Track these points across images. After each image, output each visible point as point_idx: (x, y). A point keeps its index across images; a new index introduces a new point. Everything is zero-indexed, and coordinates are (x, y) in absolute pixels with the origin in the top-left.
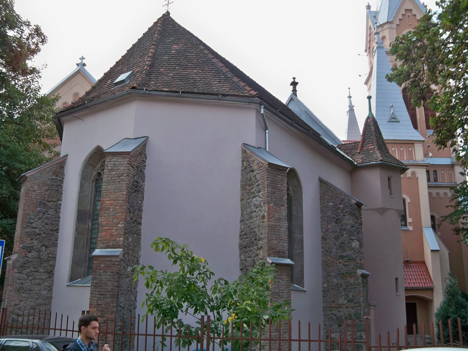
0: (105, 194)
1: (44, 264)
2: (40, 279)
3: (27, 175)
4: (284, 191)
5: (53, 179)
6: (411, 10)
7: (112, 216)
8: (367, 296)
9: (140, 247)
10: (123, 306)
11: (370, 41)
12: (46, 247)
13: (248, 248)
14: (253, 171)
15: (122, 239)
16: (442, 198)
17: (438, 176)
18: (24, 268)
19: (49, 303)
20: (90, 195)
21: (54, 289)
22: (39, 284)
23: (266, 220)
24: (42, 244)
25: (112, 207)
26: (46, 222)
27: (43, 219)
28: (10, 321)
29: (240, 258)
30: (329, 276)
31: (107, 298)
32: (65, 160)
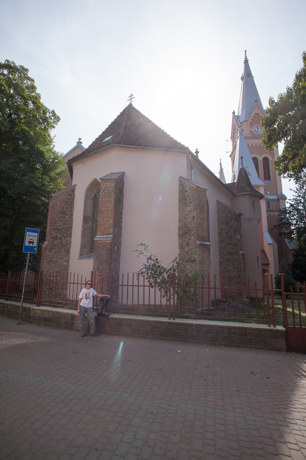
0: (101, 204)
1: (64, 247)
2: (62, 256)
3: (53, 196)
4: (205, 203)
5: (68, 198)
6: (259, 114)
7: (106, 216)
8: (245, 266)
9: (121, 236)
10: (113, 270)
11: (234, 133)
12: (65, 237)
13: (184, 236)
14: (186, 192)
15: (112, 230)
16: (272, 217)
17: (270, 205)
18: (52, 249)
19: (68, 269)
20: (90, 207)
21: (70, 261)
22: (61, 259)
23: (195, 219)
24: (63, 236)
25: (105, 211)
26: (65, 223)
27: (63, 221)
28: (45, 280)
29: (179, 242)
30: (223, 254)
31: (103, 264)
32: (75, 187)
